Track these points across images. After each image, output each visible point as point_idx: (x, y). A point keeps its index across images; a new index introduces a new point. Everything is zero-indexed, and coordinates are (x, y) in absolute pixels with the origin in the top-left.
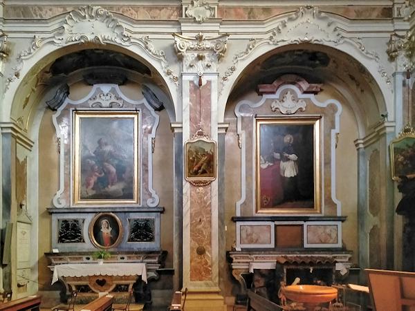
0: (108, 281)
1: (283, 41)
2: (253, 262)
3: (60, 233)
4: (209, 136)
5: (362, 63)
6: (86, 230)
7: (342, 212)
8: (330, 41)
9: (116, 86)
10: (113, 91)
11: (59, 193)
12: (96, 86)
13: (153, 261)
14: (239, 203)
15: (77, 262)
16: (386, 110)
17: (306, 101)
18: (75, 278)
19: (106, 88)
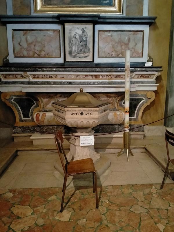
7: (14, 11)
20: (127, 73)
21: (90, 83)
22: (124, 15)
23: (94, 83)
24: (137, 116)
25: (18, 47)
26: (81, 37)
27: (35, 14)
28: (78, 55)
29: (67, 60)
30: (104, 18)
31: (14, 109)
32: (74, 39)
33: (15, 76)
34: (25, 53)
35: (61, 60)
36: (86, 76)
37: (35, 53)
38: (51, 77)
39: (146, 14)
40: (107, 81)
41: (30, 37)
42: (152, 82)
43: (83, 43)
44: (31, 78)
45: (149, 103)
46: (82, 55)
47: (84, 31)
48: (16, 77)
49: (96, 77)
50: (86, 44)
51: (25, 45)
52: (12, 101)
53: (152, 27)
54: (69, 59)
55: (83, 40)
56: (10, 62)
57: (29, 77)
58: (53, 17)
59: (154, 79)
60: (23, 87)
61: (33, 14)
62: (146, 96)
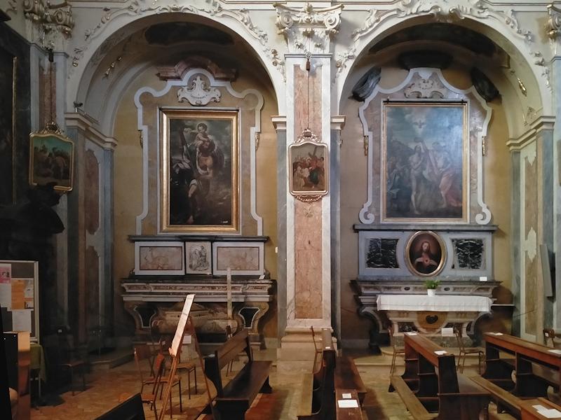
0: (440, 317)
1: (150, 9)
2: (381, 294)
3: (369, 255)
4: (319, 137)
5: (510, 40)
6: (401, 252)
7: (142, 231)
8: (203, 10)
9: (438, 71)
10: (434, 76)
11: (367, 205)
12: (412, 71)
13: (264, 292)
14: (139, 218)
15: (389, 292)
16: (541, 104)
17: (219, 90)
18: (401, 313)
19: (425, 73)
20: (229, 286)
21: (206, 294)
22: (241, 234)
23: (210, 294)
24: (253, 326)
25: (143, 261)
26: (200, 253)
27: (161, 234)
28: (198, 268)
29: (187, 273)
30: (221, 237)
31: (135, 317)
32: (194, 255)
33: (138, 287)
34: (150, 267)
35: (182, 273)
36: (203, 287)
37: (159, 266)
38: (170, 288)
39: (260, 234)
40: (223, 292)
41: (155, 253)
42: (265, 294)
43: (203, 258)
44: (152, 289)
45: (263, 314)
46: (202, 268)
47: (203, 248)
48: (140, 289)
49: (213, 288)
50: (205, 259)
51: (150, 259)
52: (134, 310)
53: (266, 244)
54: (189, 271)
55: (202, 256)
56: (136, 274)
57: (152, 287)
58: (176, 237)
59: (266, 291)
60: (143, 297)
61: (159, 233)
62: (260, 307)
